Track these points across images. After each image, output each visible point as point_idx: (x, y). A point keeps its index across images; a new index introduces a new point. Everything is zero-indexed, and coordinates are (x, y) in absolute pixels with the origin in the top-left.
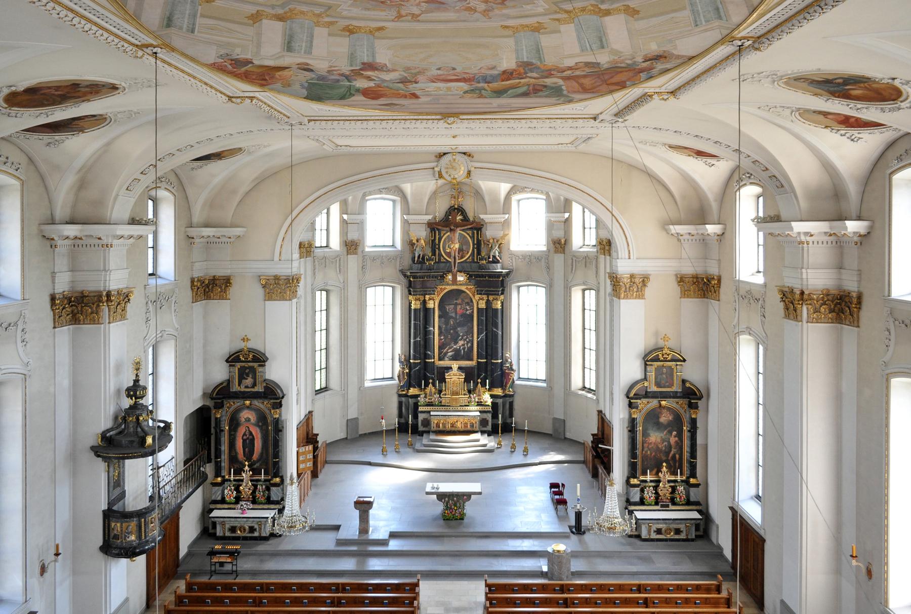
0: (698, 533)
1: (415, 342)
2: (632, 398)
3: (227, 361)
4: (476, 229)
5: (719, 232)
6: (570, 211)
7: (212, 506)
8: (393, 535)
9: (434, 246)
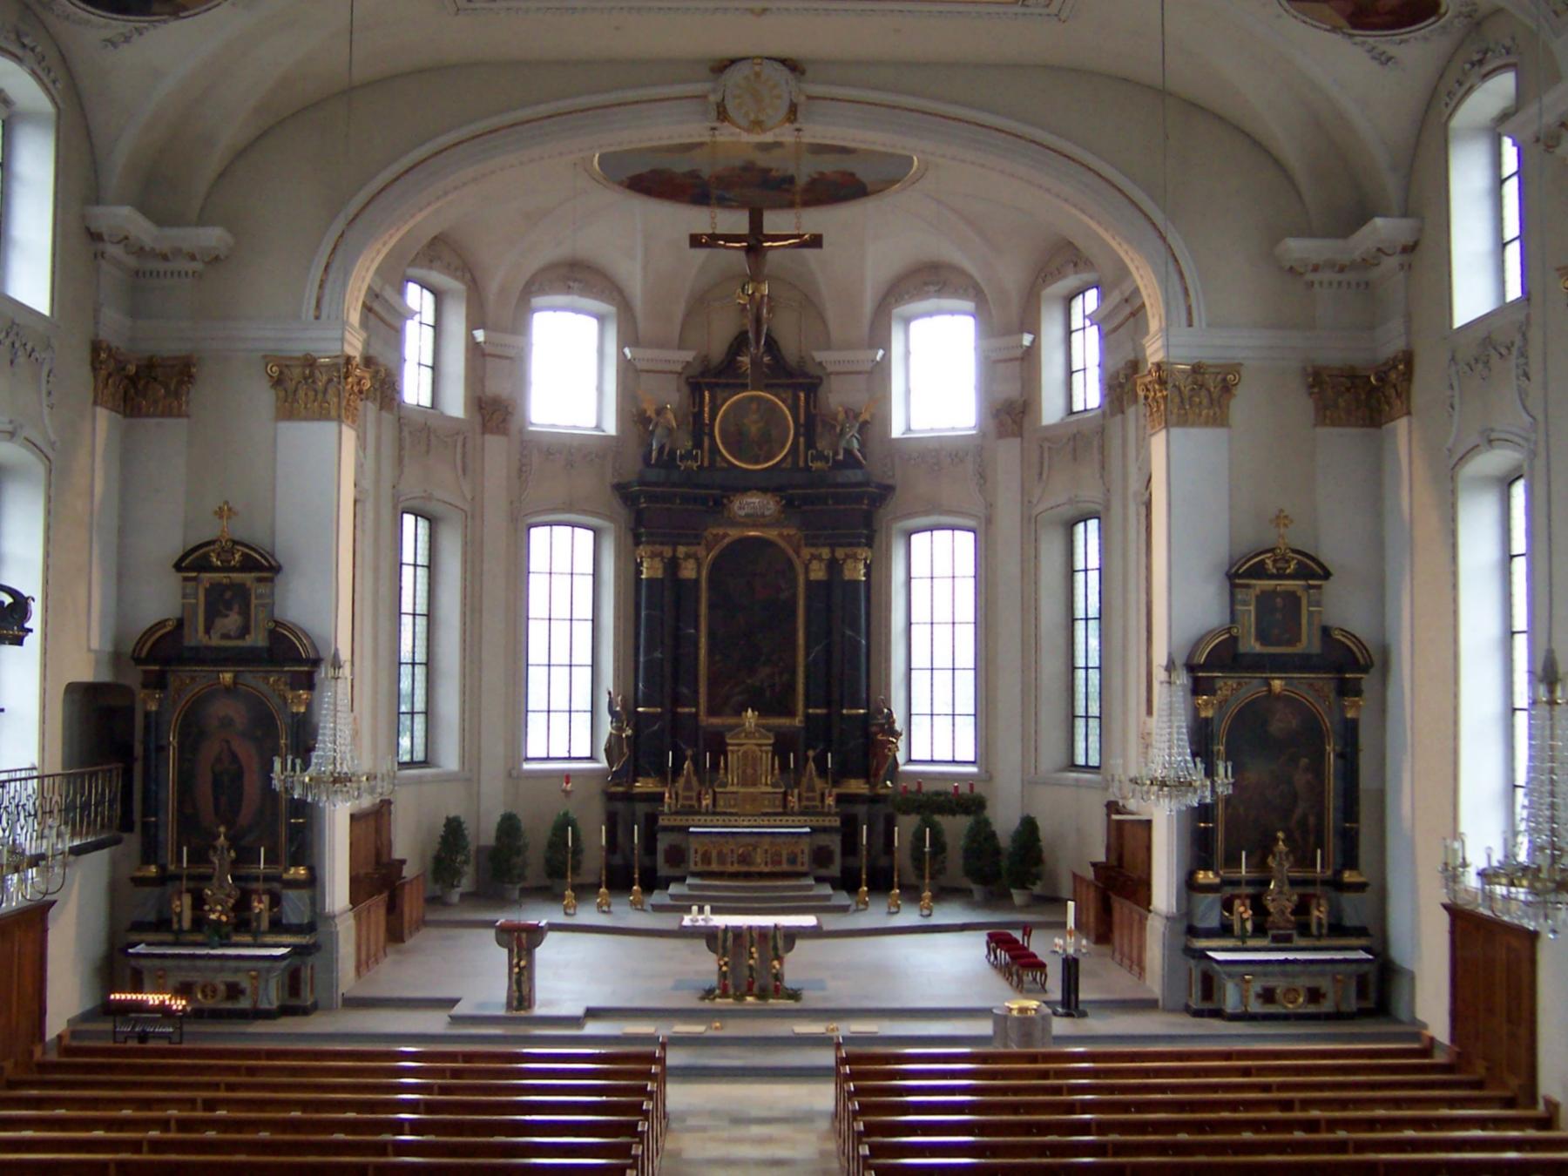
0: (1365, 1005)
1: (648, 663)
2: (1202, 667)
3: (178, 567)
4: (801, 386)
5: (1407, 239)
6: (1036, 332)
7: (134, 937)
8: (593, 1013)
9: (699, 429)
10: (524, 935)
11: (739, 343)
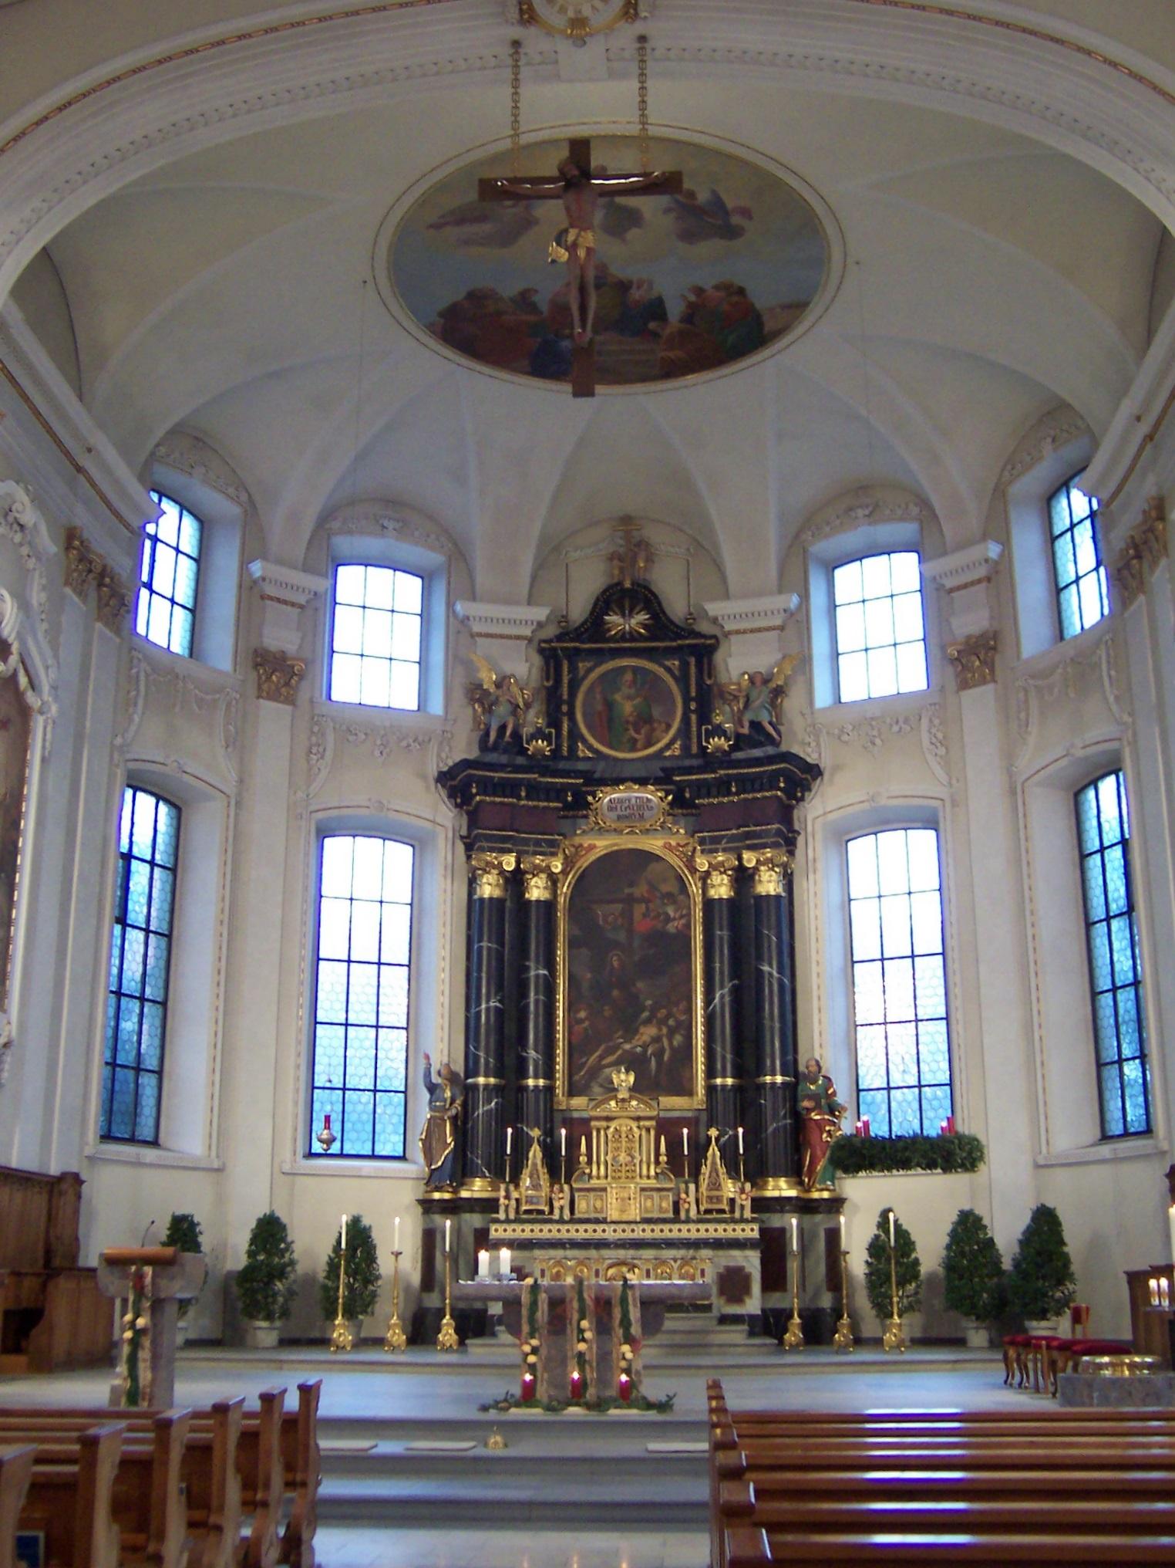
4: (694, 650)
6: (1006, 543)
10: (148, 1270)
11: (612, 598)
